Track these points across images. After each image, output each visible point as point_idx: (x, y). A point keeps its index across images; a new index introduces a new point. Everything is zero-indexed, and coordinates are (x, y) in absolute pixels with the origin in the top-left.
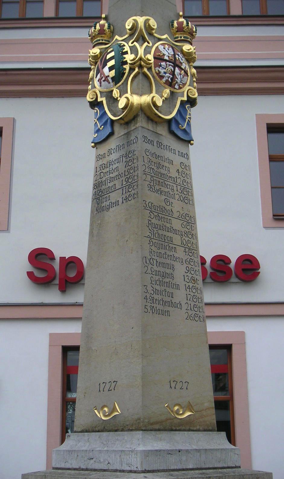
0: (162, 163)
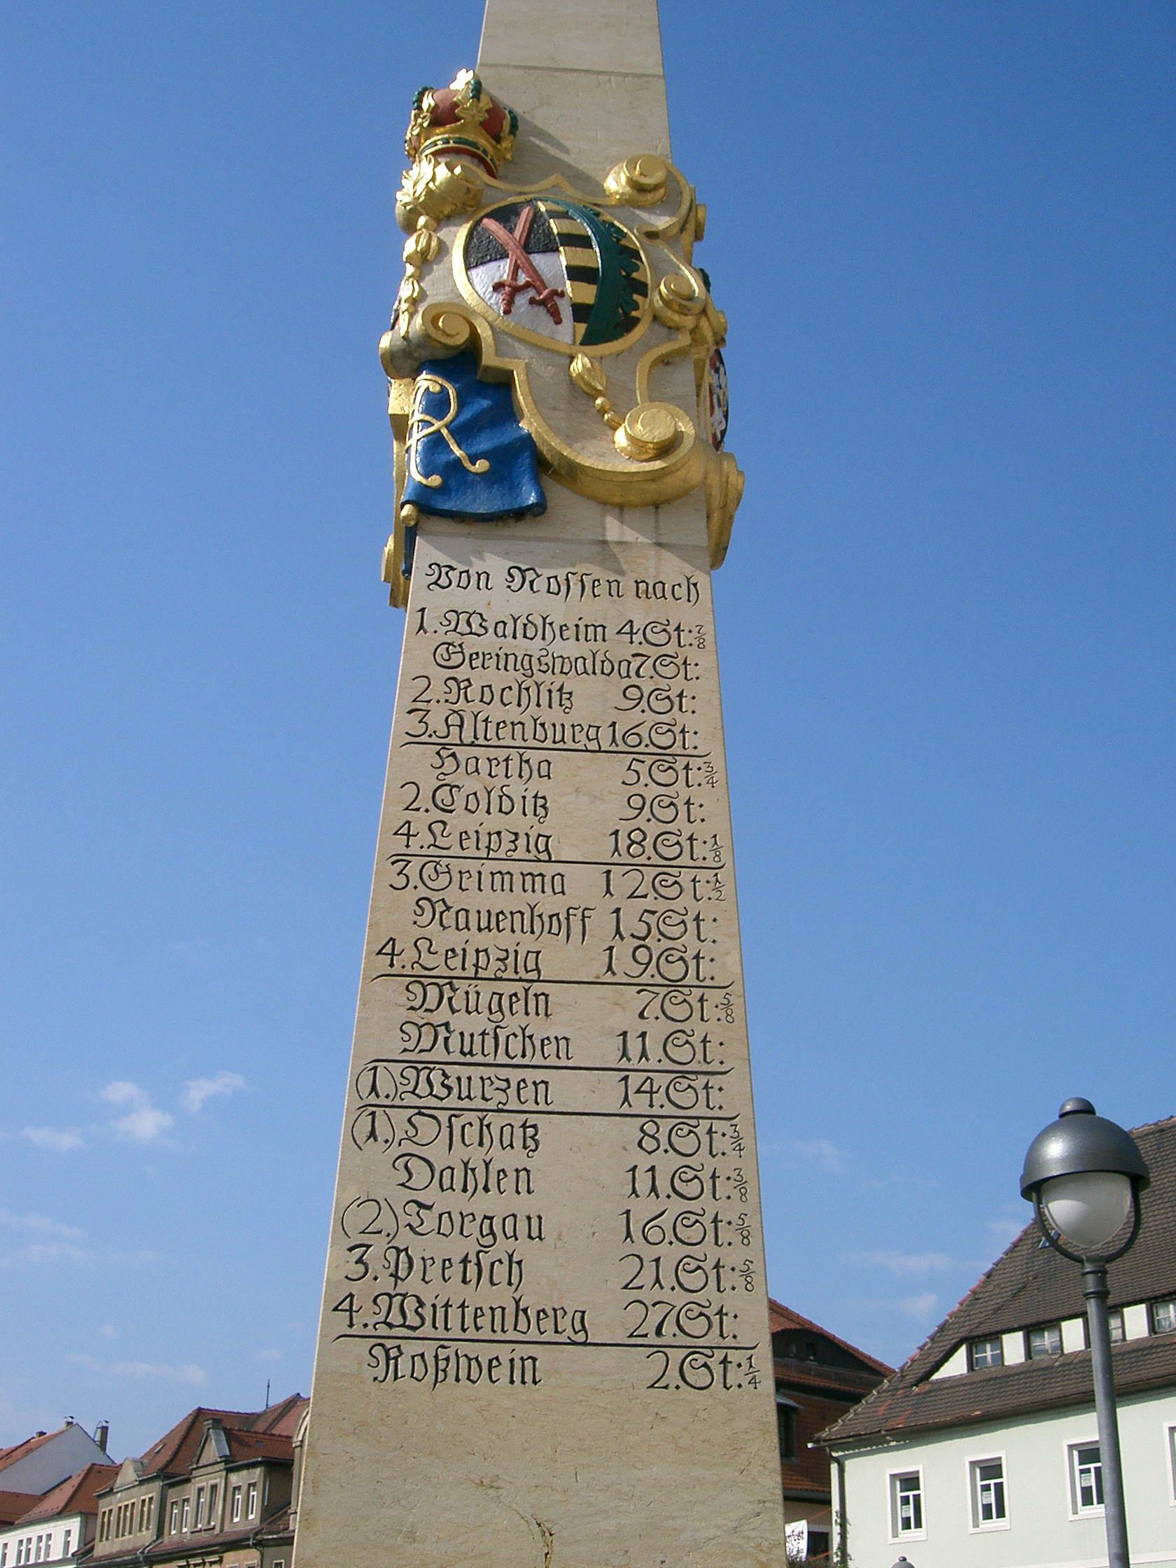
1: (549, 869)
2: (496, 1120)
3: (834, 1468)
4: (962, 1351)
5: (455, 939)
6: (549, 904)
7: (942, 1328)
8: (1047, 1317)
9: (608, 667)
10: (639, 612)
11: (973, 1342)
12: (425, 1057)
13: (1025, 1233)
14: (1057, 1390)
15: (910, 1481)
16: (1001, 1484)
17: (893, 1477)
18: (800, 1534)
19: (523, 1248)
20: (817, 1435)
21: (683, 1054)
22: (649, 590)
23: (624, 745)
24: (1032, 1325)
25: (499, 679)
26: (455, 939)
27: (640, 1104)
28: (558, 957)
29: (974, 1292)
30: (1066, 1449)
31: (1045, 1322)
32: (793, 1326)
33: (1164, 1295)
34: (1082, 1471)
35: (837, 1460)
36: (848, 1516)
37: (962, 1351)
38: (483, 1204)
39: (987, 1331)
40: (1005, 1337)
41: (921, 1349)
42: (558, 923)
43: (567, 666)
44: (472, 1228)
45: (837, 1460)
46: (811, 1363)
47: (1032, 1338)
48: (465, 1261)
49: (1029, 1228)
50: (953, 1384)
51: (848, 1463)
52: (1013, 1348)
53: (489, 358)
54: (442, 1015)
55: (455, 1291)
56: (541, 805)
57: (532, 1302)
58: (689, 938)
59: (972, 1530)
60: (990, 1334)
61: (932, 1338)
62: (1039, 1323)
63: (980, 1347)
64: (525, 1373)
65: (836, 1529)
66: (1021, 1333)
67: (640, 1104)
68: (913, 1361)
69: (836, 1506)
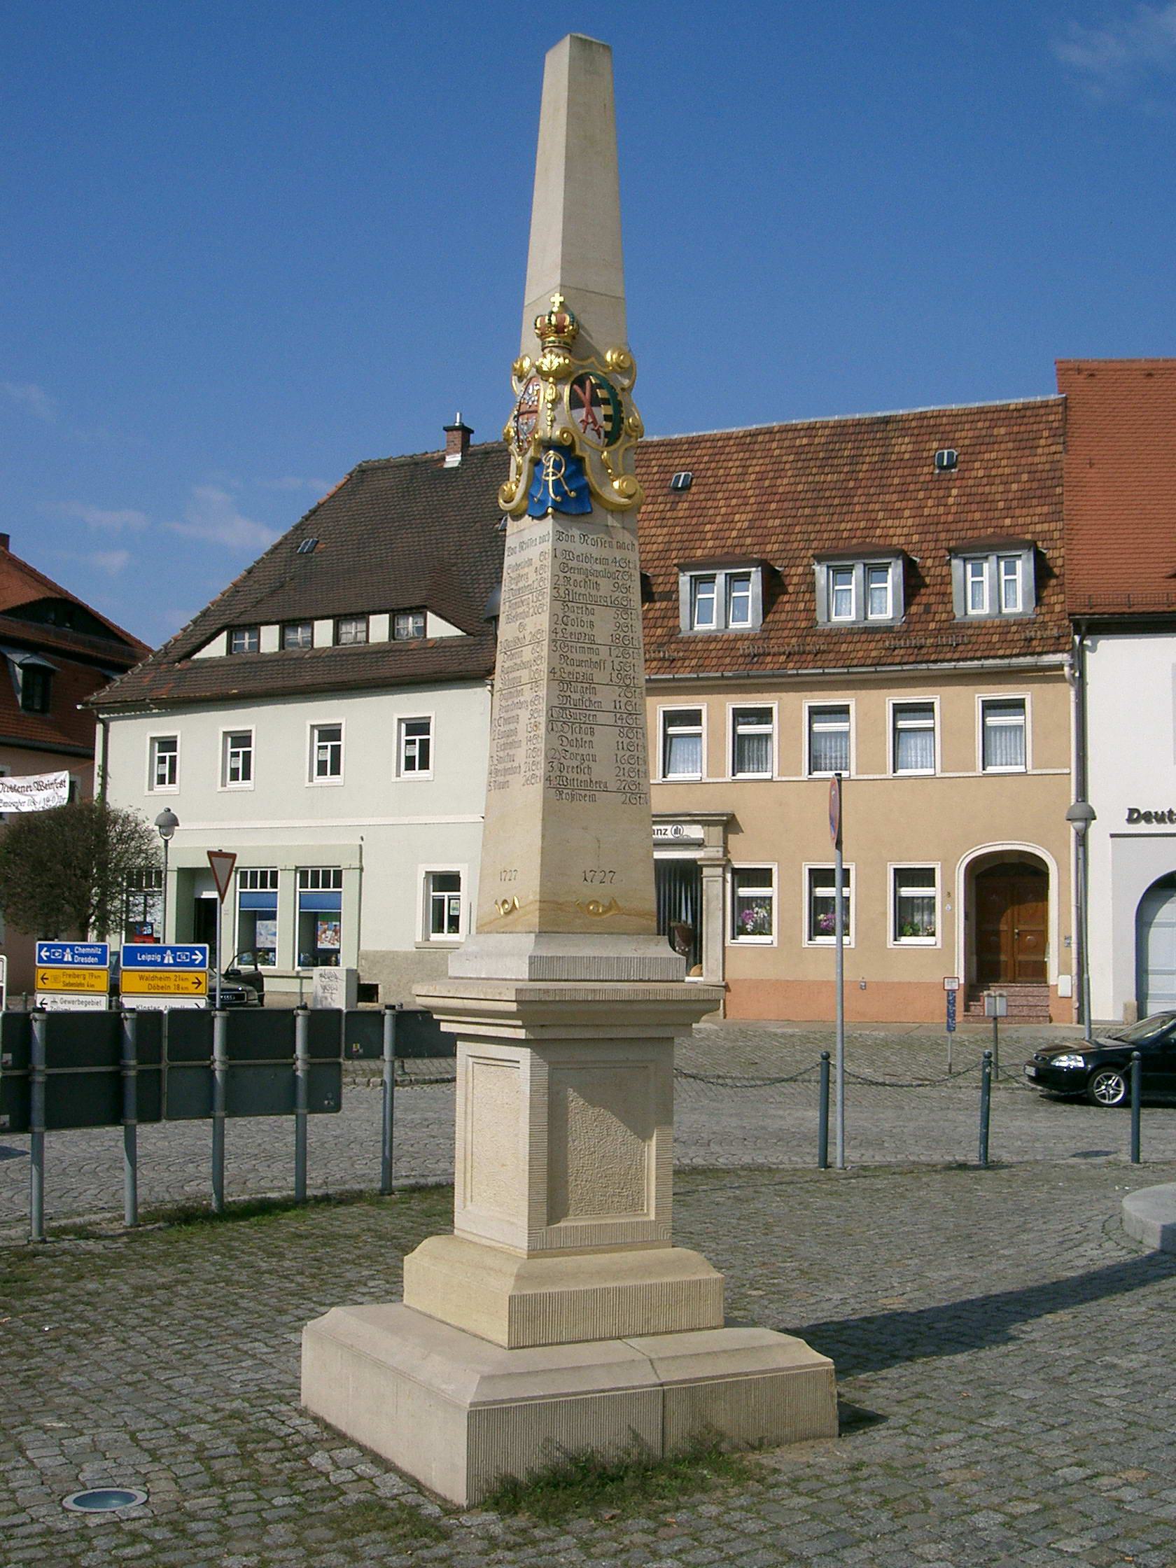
1: (595, 647)
3: (99, 728)
4: (223, 637)
5: (570, 669)
6: (595, 658)
7: (205, 614)
8: (302, 616)
9: (610, 576)
10: (618, 554)
11: (234, 629)
13: (285, 538)
14: (307, 678)
15: (168, 744)
17: (153, 739)
18: (62, 783)
19: (592, 764)
20: (85, 699)
21: (630, 708)
22: (621, 546)
23: (613, 604)
24: (289, 621)
25: (580, 578)
26: (570, 669)
27: (619, 723)
28: (599, 676)
29: (235, 585)
30: (309, 728)
31: (301, 619)
32: (54, 595)
33: (405, 609)
34: (320, 747)
35: (102, 721)
36: (110, 770)
37: (223, 637)
38: (581, 751)
39: (247, 622)
40: (263, 629)
41: (184, 630)
42: (597, 665)
43: (597, 574)
45: (102, 721)
46: (67, 629)
47: (287, 632)
49: (289, 534)
50: (211, 663)
51: (112, 725)
52: (269, 639)
53: (578, 452)
54: (568, 693)
55: (575, 776)
56: (592, 624)
59: (220, 789)
60: (250, 625)
61: (195, 622)
62: (294, 620)
63: (239, 635)
64: (593, 799)
65: (97, 781)
66: (277, 627)
67: (619, 723)
68: (176, 640)
69: (98, 760)
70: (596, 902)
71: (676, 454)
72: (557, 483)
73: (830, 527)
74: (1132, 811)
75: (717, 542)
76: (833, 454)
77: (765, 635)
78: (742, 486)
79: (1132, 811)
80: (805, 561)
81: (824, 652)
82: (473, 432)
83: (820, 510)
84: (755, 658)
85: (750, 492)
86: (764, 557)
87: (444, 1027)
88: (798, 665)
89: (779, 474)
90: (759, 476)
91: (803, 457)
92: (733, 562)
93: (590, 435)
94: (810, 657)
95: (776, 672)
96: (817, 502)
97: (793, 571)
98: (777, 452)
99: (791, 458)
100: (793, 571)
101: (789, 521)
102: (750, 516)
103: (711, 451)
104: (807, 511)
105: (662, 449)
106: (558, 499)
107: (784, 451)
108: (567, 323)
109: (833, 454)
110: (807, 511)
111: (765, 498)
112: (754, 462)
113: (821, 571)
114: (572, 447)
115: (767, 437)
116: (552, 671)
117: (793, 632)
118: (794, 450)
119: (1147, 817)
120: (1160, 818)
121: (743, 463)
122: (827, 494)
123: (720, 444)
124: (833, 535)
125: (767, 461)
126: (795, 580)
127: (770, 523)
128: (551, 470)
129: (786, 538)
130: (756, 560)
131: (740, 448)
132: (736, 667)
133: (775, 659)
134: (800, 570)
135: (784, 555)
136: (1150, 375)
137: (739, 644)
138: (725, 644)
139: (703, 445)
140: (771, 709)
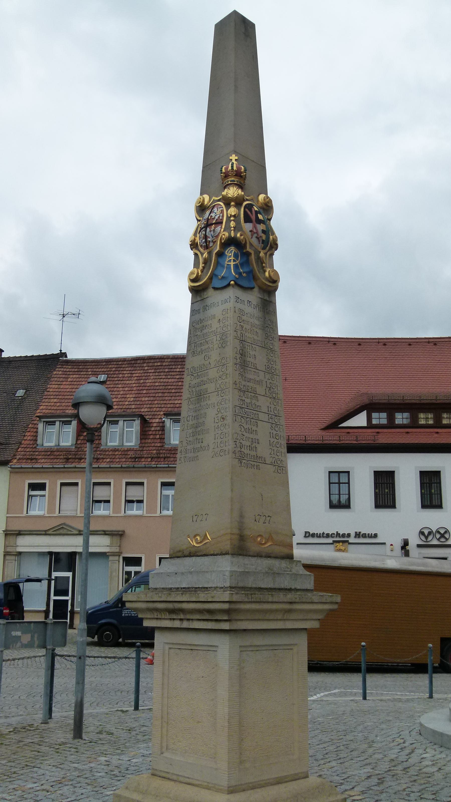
0: (205, 324)
2: (252, 420)
6: (258, 379)
12: (242, 406)
16: (135, 572)
19: (257, 445)
21: (276, 412)
26: (243, 383)
28: (260, 390)
44: (250, 440)
48: (138, 739)
54: (243, 398)
57: (259, 455)
58: (276, 389)
70: (260, 536)
71: (99, 367)
72: (236, 266)
73: (171, 402)
74: (306, 532)
75: (119, 407)
76: (172, 370)
77: (141, 449)
78: (130, 382)
79: (306, 532)
80: (159, 417)
81: (168, 457)
82: (3, 351)
83: (166, 394)
84: (136, 459)
85: (134, 385)
86: (141, 413)
87: (146, 624)
88: (157, 463)
89: (147, 378)
90: (138, 378)
91: (158, 371)
92: (129, 416)
93: (254, 241)
94: (162, 460)
95: (147, 466)
96: (165, 391)
97: (154, 421)
98: (146, 368)
99: (153, 371)
100: (154, 421)
101: (152, 399)
102: (134, 396)
103: (116, 366)
104: (160, 395)
105: (93, 364)
106: (237, 276)
107: (149, 368)
108: (243, 170)
109: (172, 370)
110: (160, 395)
111: (141, 388)
112: (136, 372)
113: (168, 422)
114: (245, 246)
115: (142, 361)
116: (235, 383)
117: (154, 448)
118: (154, 368)
119: (313, 535)
120: (319, 536)
121: (131, 372)
122: (169, 387)
123: (120, 363)
124: (172, 406)
125: (142, 372)
126: (155, 425)
127: (143, 399)
128: (232, 258)
129: (151, 406)
130: (138, 415)
131: (129, 365)
132: (128, 463)
133: (146, 460)
134: (157, 420)
135: (150, 413)
136: (310, 343)
137: (129, 453)
138: (124, 452)
139: (112, 363)
140: (144, 482)
